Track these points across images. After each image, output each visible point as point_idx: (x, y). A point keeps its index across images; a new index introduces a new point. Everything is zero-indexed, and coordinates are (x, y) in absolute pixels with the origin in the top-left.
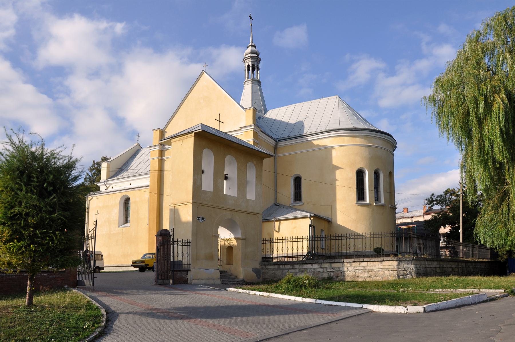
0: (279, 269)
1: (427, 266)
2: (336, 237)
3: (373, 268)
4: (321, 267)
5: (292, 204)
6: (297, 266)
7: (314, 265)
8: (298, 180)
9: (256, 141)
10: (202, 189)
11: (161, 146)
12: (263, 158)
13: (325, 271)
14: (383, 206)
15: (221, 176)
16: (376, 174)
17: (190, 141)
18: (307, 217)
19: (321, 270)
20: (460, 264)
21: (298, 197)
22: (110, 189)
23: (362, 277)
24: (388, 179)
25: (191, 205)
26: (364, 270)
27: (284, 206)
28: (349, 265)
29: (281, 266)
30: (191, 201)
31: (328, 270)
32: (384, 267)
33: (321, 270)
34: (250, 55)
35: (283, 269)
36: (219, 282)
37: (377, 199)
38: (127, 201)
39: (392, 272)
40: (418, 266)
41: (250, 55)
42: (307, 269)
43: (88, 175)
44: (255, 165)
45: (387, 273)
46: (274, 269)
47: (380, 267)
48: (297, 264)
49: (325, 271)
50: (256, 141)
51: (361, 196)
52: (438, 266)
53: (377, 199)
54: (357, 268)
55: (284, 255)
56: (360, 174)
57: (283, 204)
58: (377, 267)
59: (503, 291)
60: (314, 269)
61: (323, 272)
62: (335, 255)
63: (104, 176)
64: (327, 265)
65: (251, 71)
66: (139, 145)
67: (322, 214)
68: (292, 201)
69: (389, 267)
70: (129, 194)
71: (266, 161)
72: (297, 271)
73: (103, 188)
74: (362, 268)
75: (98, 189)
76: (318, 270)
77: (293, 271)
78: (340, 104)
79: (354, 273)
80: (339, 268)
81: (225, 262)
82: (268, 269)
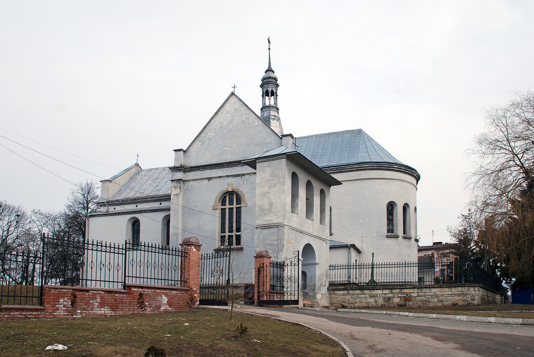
0: (349, 294)
3: (443, 293)
4: (392, 293)
6: (366, 292)
19: (391, 295)
29: (351, 292)
31: (399, 296)
35: (353, 295)
46: (343, 295)
47: (450, 293)
58: (447, 293)
72: (368, 296)
76: (388, 295)
82: (337, 294)
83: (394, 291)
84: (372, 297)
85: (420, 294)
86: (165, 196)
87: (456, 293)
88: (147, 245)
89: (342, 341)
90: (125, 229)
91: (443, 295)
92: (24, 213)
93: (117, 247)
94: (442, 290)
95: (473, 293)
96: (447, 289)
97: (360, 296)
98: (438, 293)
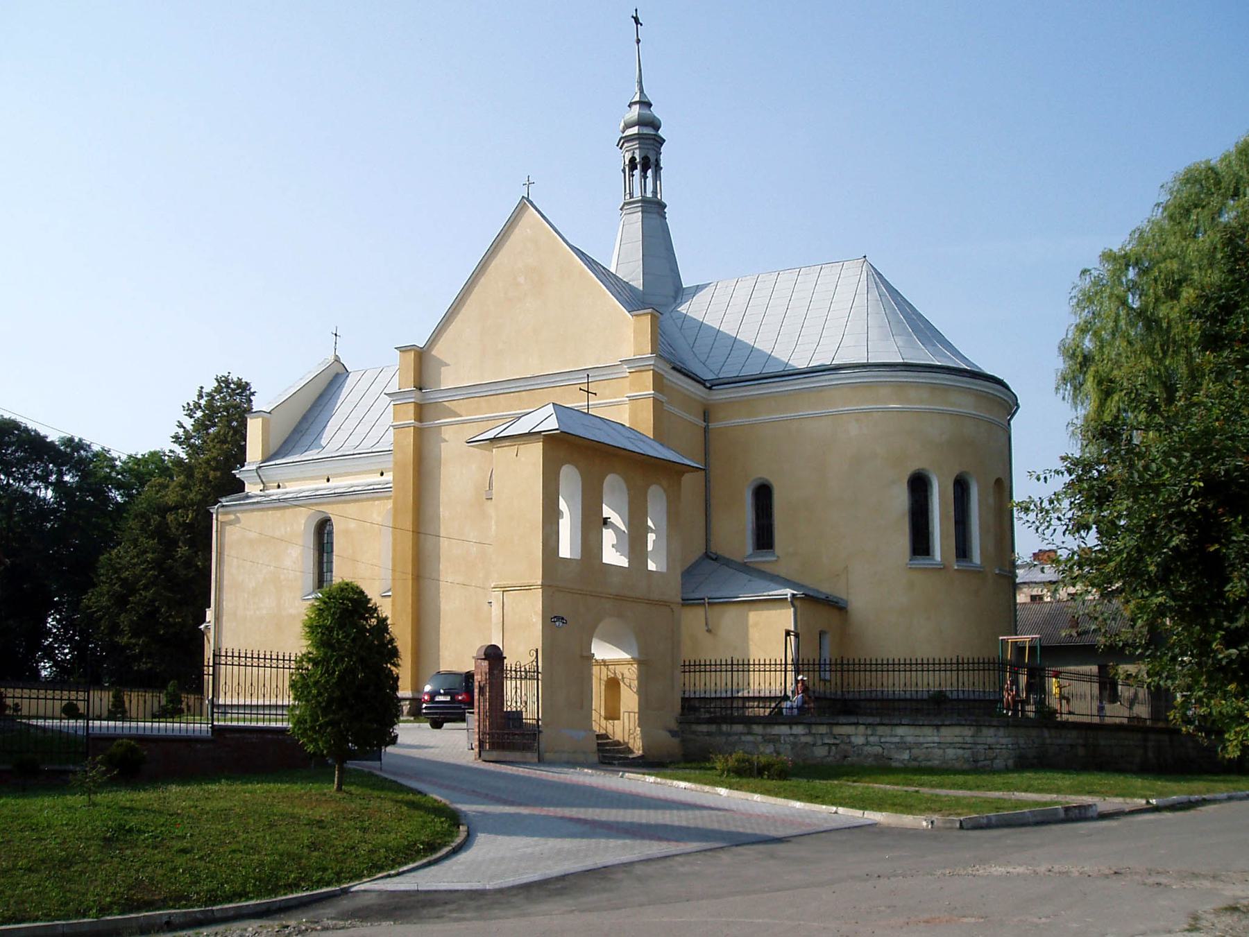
0: (721, 733)
1: (1048, 741)
2: (842, 664)
3: (921, 740)
4: (810, 734)
5: (750, 556)
6: (757, 729)
7: (794, 727)
8: (763, 494)
9: (660, 396)
10: (561, 555)
11: (418, 392)
12: (683, 473)
13: (819, 742)
14: (978, 572)
15: (593, 523)
16: (961, 487)
17: (536, 451)
18: (781, 601)
19: (809, 739)
20: (1152, 737)
21: (764, 538)
22: (274, 492)
23: (897, 760)
24: (991, 500)
25: (539, 592)
26: (902, 745)
27: (727, 562)
28: (869, 732)
29: (724, 728)
30: (540, 582)
31: (826, 741)
32: (943, 740)
33: (809, 739)
34: (635, 130)
35: (729, 735)
36: (595, 758)
37: (963, 551)
38: (323, 532)
39: (960, 752)
40: (1021, 741)
41: (635, 130)
42: (779, 736)
43: (181, 426)
44: (665, 491)
45: (951, 752)
46: (709, 734)
47: (936, 739)
48: (759, 724)
49: (819, 742)
50: (660, 396)
51: (920, 544)
52: (1081, 741)
53: (963, 551)
54: (888, 739)
55: (729, 695)
56: (919, 485)
57: (727, 555)
58: (929, 739)
59: (1144, 802)
60: (795, 736)
61: (814, 745)
62: (857, 696)
63: (254, 451)
64: (823, 729)
65: (637, 172)
66: (337, 360)
67: (826, 588)
68: (749, 548)
69: (956, 740)
70: (332, 511)
71: (687, 478)
72: (759, 738)
73: (252, 488)
74: (897, 740)
75: (239, 486)
76: (803, 739)
77: (750, 738)
78: (861, 300)
79: (880, 750)
80: (849, 736)
81: (603, 713)
82: (694, 732)
83: (814, 730)
84: (769, 741)
85: (871, 739)
86: (688, 605)
87: (949, 740)
88: (281, 657)
89: (459, 802)
90: (540, 634)
91: (922, 744)
92: (1063, 459)
93: (281, 657)
94: (918, 731)
95: (989, 740)
96: (928, 731)
97: (743, 738)
98: (909, 739)
